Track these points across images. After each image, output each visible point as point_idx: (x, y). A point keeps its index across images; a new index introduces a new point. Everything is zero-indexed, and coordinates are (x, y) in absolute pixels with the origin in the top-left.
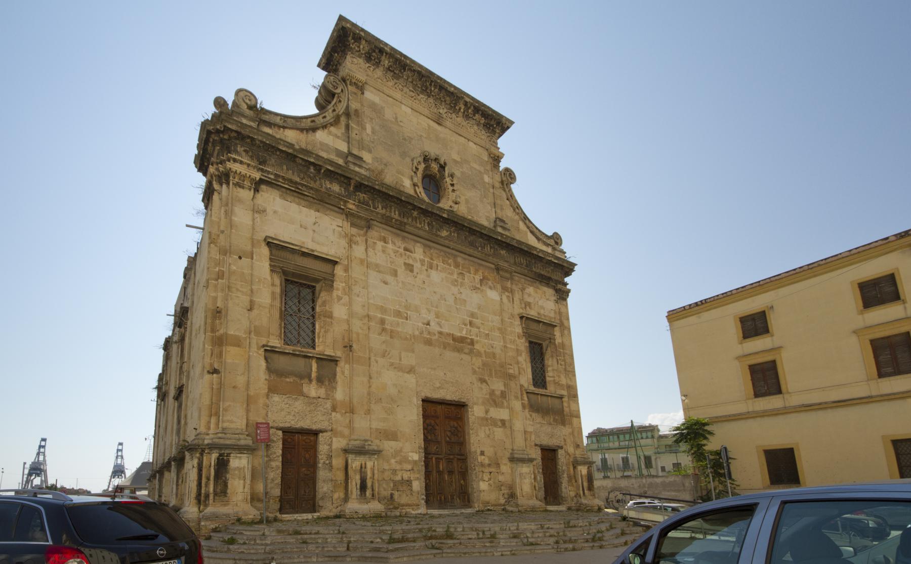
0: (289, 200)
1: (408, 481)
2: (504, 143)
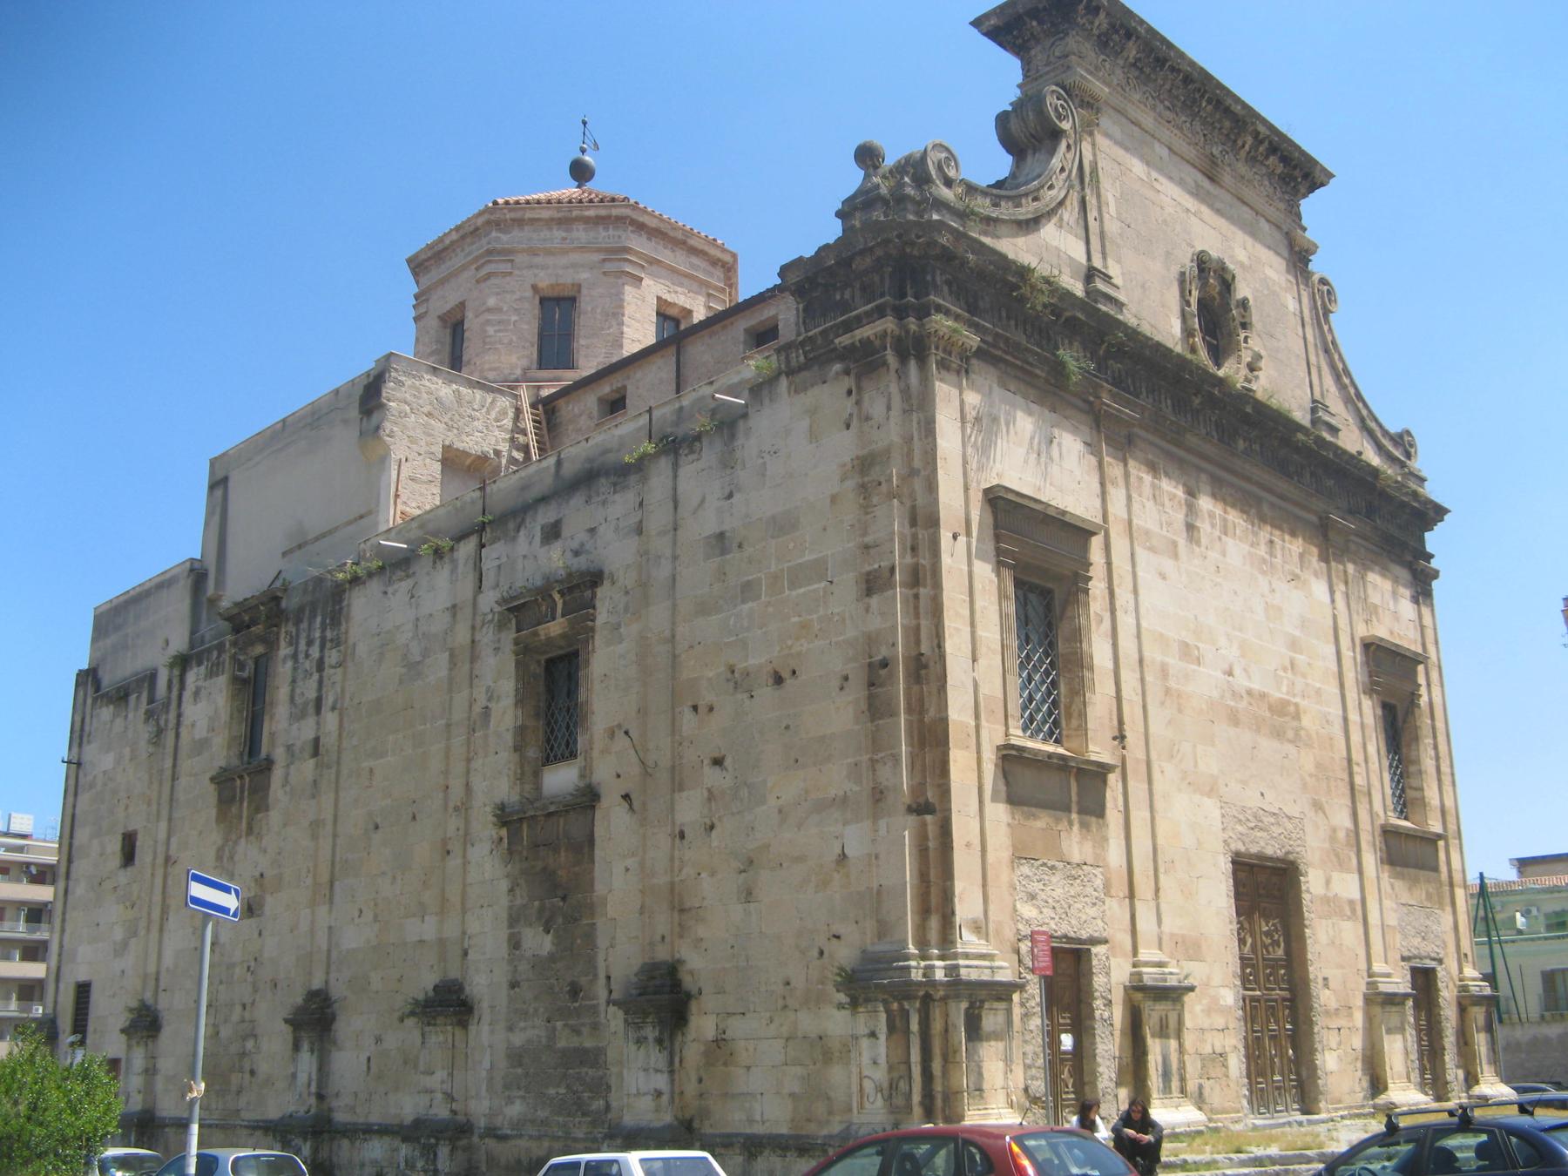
0: (1012, 389)
1: (1221, 1055)
2: (1312, 207)
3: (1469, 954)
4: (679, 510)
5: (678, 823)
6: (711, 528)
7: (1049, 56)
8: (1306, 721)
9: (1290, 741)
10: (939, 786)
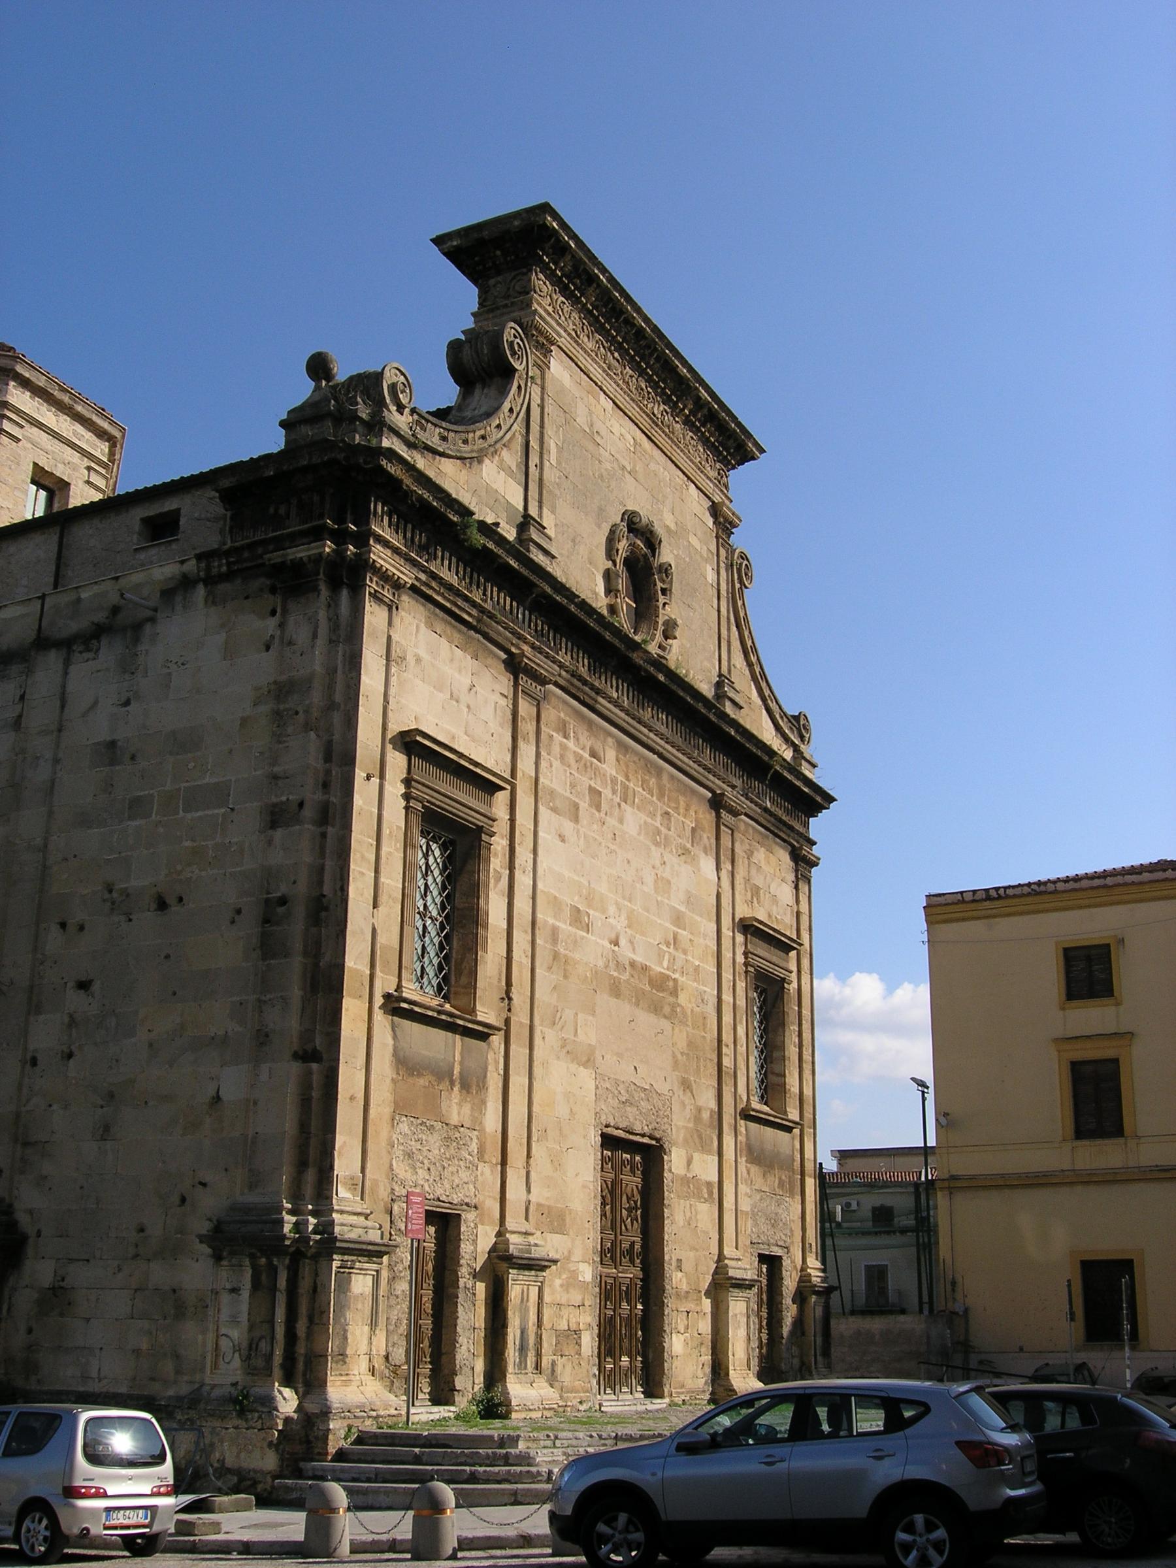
3: (814, 1244)
4: (66, 711)
5: (31, 1047)
6: (104, 736)
7: (509, 289)
8: (683, 999)
9: (665, 1017)
10: (328, 1034)
